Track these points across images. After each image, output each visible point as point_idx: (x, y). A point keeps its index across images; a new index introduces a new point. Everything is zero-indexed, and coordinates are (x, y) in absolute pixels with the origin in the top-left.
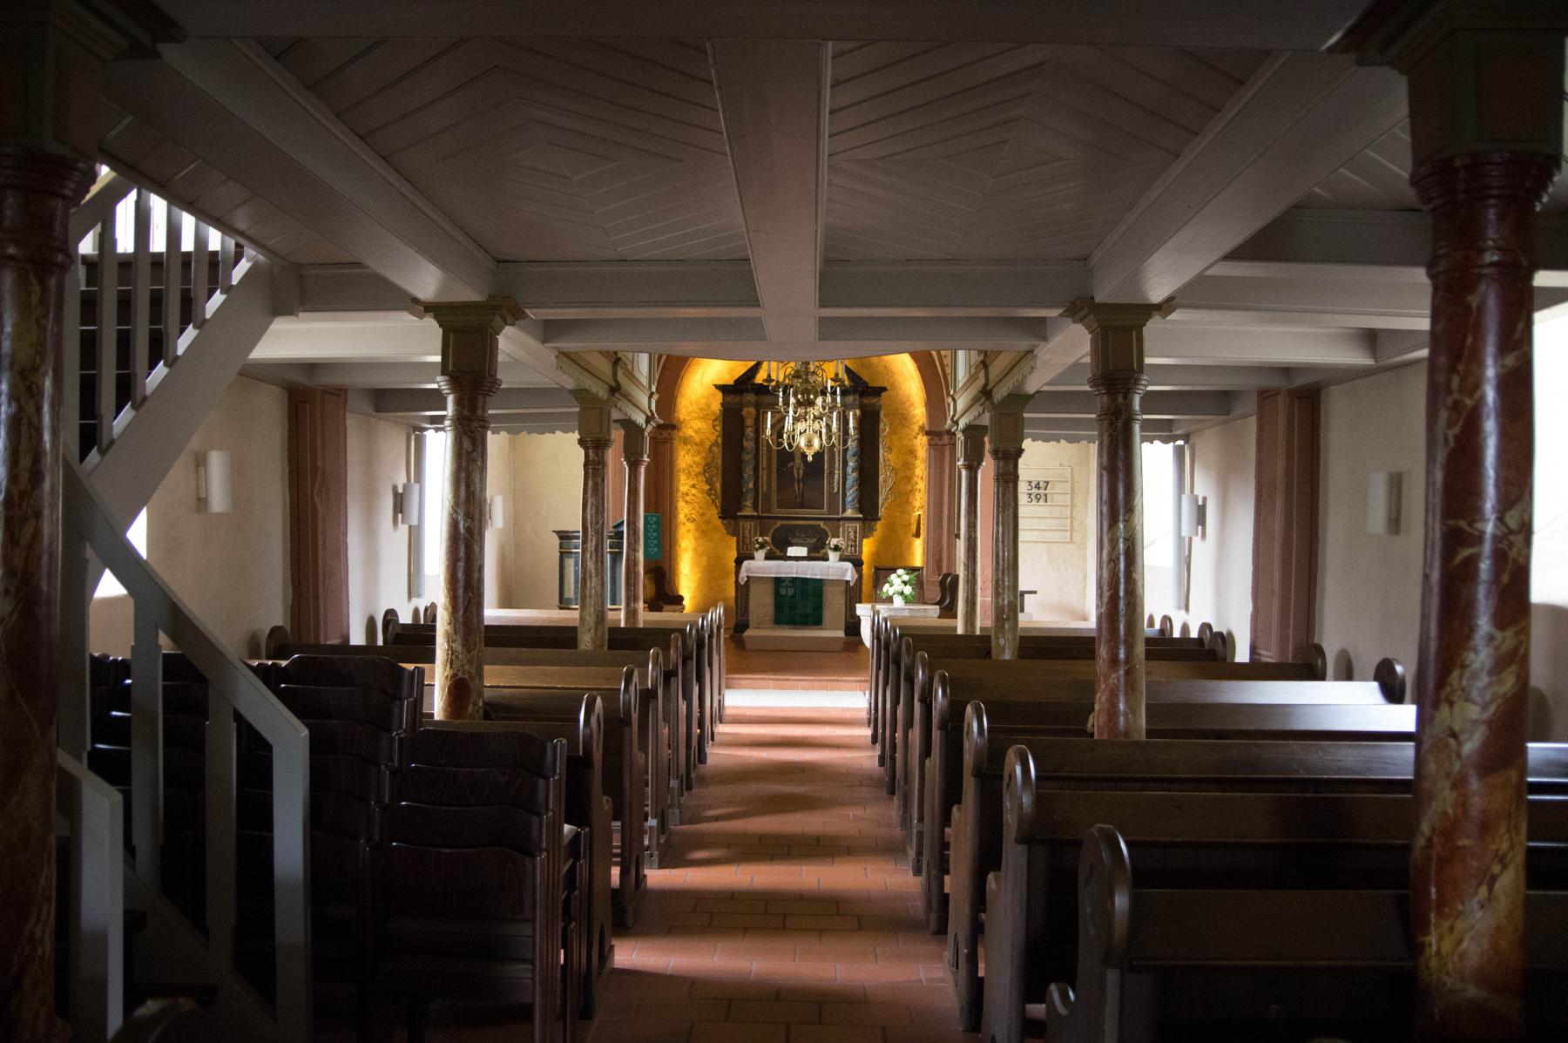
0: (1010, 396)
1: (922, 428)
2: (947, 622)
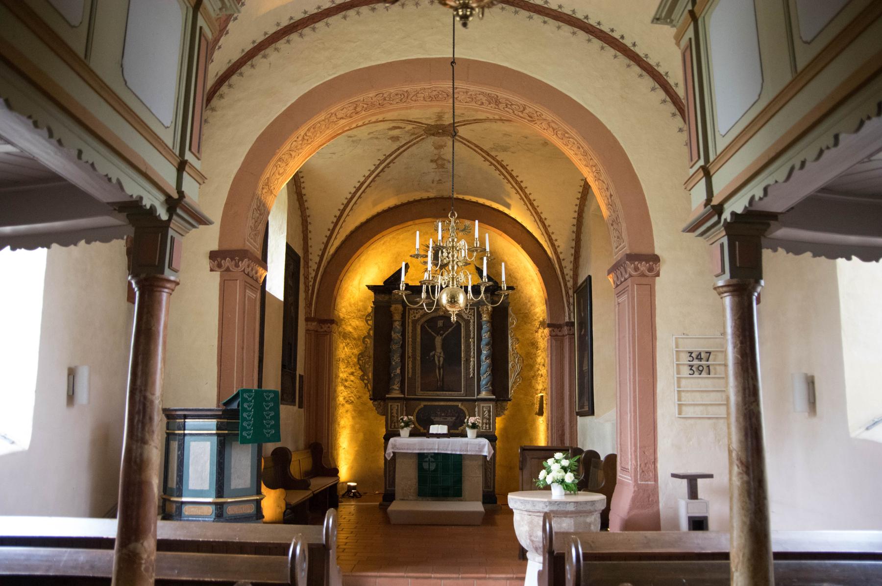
1: (542, 324)
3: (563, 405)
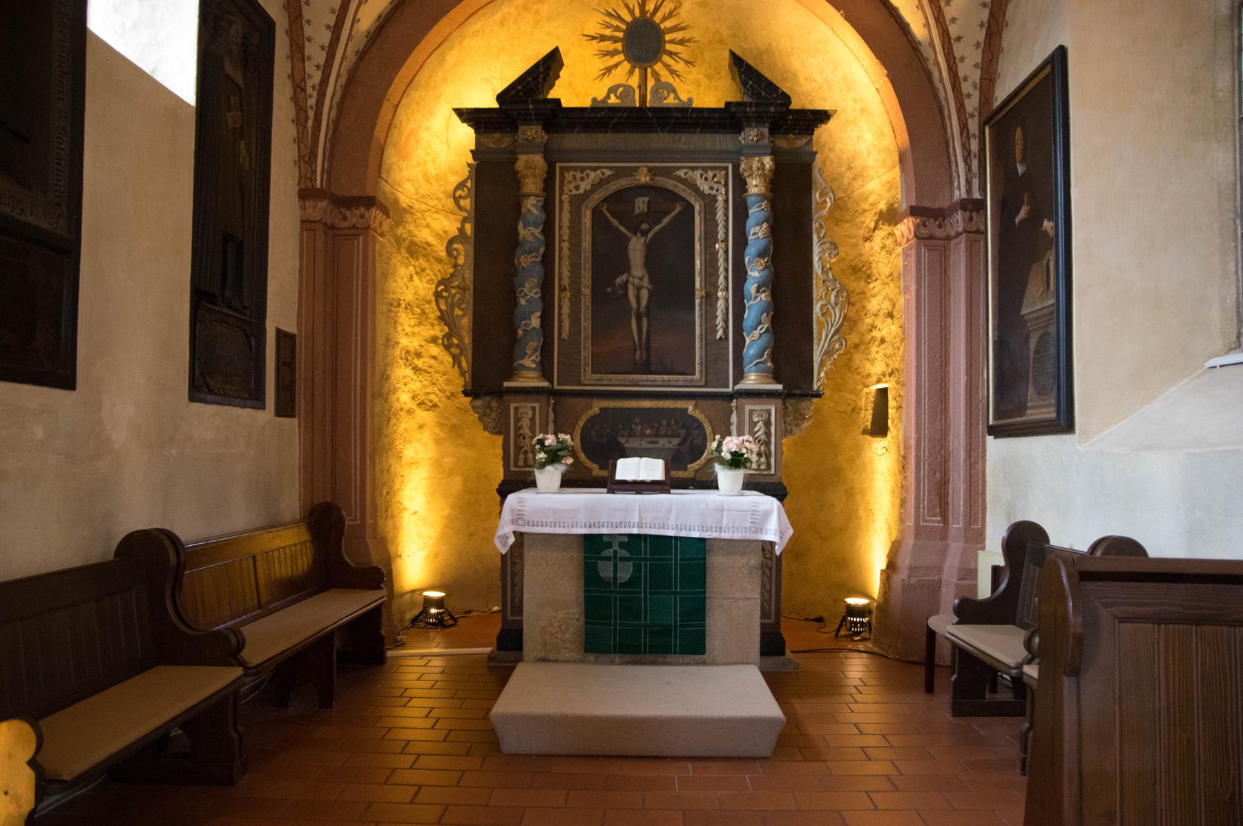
3: (945, 411)
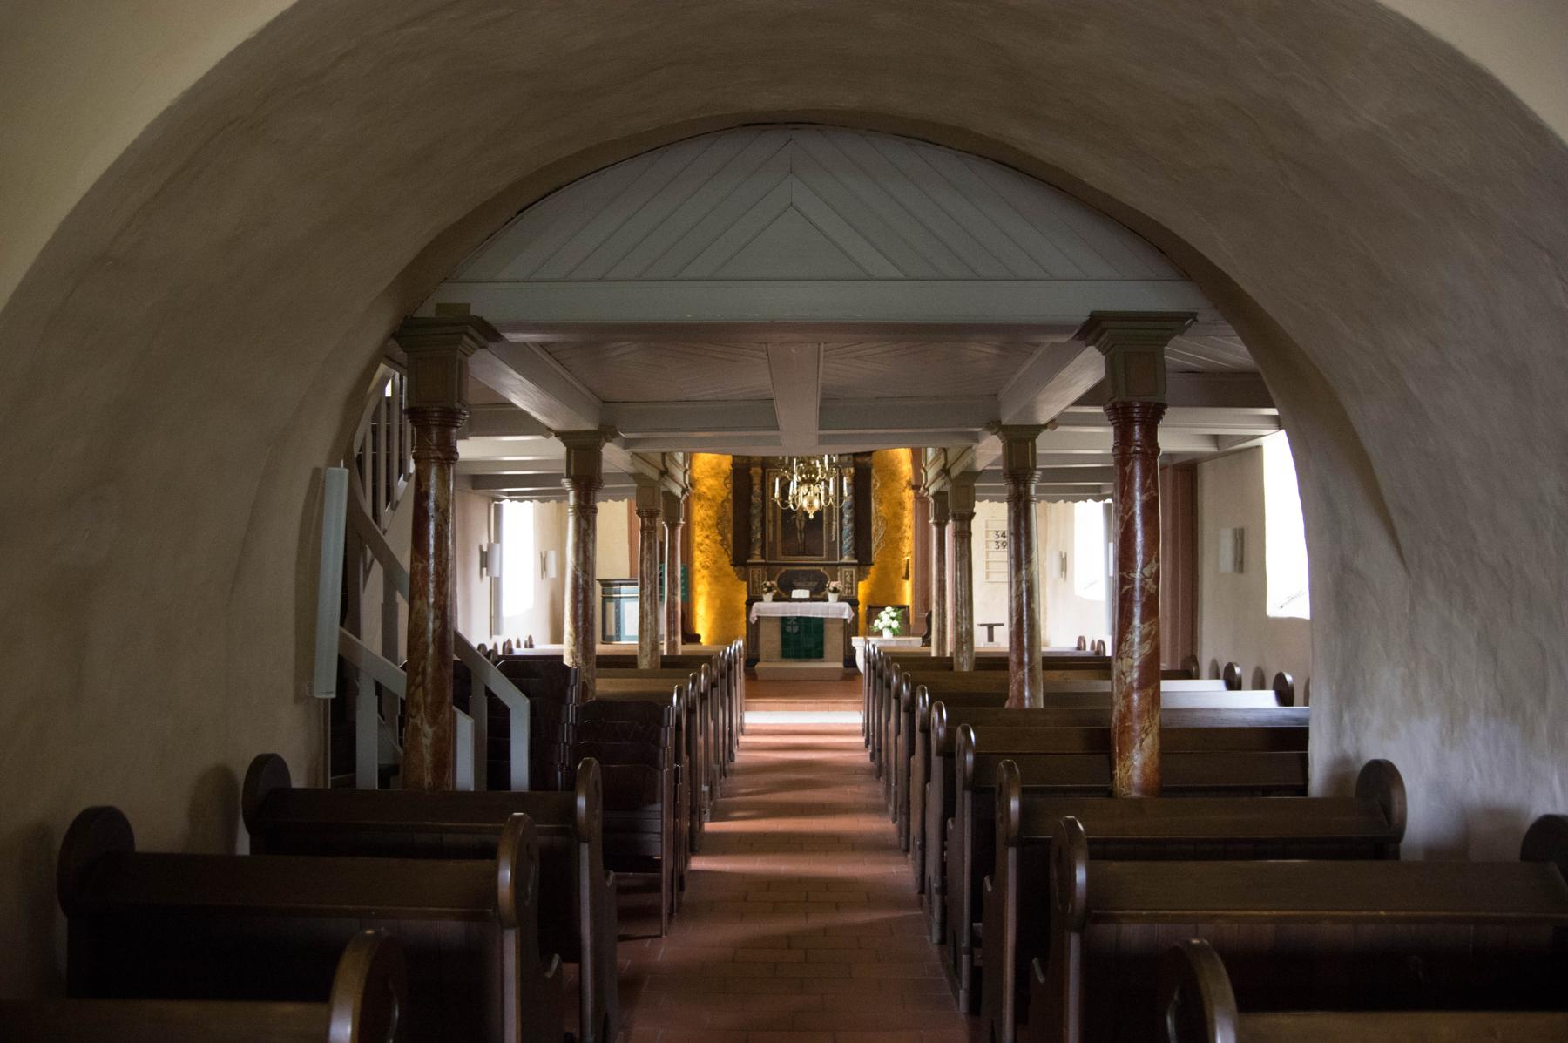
0: (962, 473)
1: (909, 483)
2: (925, 649)
